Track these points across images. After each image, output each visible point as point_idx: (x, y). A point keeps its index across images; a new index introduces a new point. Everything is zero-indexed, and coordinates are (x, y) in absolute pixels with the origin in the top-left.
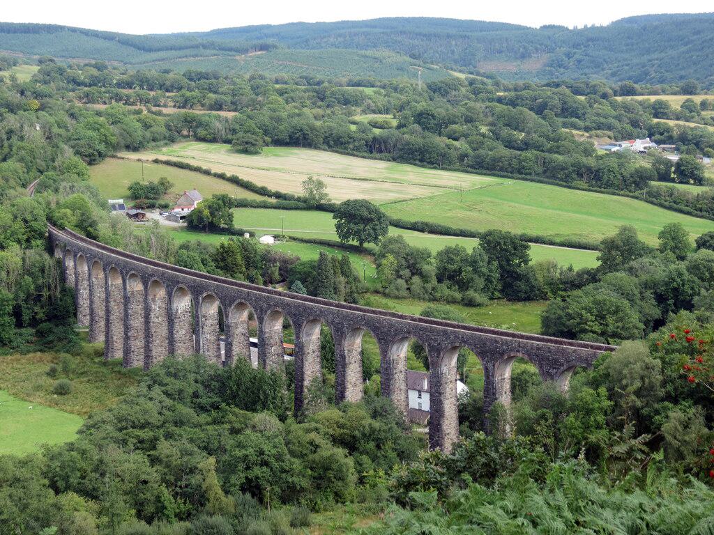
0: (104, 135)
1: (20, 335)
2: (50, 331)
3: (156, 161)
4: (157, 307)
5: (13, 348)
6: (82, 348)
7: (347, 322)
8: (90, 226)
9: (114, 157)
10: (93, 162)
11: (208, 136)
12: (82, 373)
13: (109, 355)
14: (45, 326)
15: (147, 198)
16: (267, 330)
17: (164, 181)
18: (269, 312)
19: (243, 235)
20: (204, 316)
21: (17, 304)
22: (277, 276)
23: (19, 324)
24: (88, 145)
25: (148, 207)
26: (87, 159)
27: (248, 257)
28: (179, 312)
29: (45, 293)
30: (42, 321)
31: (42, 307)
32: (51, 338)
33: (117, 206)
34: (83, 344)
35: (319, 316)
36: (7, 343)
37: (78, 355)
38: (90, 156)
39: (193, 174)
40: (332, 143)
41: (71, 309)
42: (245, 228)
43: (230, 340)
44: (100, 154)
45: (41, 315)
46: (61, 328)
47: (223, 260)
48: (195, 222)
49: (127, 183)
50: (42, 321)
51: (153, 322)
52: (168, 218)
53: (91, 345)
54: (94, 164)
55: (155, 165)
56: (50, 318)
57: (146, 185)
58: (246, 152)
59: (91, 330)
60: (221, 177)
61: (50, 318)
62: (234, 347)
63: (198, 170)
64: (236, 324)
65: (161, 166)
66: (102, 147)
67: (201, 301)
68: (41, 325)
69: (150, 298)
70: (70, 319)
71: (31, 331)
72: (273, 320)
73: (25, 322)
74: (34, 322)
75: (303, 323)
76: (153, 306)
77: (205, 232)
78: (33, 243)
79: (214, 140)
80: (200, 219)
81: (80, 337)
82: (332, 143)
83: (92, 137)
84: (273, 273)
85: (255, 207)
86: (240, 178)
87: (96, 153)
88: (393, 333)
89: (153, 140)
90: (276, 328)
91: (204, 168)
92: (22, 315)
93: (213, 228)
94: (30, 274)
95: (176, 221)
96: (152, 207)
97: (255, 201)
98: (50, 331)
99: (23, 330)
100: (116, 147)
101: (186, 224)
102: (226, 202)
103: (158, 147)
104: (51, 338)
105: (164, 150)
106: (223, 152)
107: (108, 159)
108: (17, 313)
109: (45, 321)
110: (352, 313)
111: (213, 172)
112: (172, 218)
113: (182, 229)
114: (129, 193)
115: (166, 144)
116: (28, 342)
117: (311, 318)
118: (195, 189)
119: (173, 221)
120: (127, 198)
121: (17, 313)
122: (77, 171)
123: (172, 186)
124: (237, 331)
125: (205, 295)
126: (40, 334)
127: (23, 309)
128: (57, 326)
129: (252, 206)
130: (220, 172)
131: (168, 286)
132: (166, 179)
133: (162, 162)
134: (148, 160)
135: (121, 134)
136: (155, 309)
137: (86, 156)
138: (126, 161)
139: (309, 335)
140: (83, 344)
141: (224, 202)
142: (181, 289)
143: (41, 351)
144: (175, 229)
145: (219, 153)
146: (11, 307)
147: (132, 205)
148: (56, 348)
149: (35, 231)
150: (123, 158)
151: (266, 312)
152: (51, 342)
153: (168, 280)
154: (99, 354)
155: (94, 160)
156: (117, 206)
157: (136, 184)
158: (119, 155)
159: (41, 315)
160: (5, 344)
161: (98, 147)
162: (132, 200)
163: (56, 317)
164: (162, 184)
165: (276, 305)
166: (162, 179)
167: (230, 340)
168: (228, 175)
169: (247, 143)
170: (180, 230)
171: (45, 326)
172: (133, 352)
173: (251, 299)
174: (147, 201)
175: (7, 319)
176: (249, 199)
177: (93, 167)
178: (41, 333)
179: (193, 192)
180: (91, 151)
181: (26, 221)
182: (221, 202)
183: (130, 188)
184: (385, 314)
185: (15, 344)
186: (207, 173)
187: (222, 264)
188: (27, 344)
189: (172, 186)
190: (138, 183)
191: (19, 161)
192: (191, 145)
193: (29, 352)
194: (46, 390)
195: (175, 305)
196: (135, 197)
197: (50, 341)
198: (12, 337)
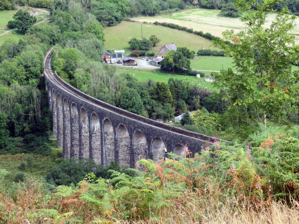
0: (121, 6)
1: (13, 141)
2: (32, 139)
3: (156, 24)
4: (85, 126)
5: (7, 150)
6: (51, 151)
7: (173, 140)
8: (72, 70)
9: (128, 20)
10: (111, 24)
11: (208, 5)
12: (42, 168)
13: (65, 156)
14: (29, 136)
15: (141, 49)
16: (135, 144)
17: (153, 38)
18: (135, 132)
19: (196, 75)
20: (106, 133)
21: (11, 121)
22: (198, 104)
23: (13, 135)
24: (109, 13)
25: (140, 56)
26: (107, 22)
27: (178, 92)
28: (96, 129)
29: (31, 114)
30: (28, 133)
31: (29, 124)
32: (32, 144)
33: (117, 55)
34: (53, 148)
35: (159, 135)
36: (3, 146)
37: (47, 155)
38: (109, 20)
39: (180, 32)
40: (294, 9)
41: (49, 125)
42: (198, 71)
43: (117, 150)
44: (116, 18)
45: (27, 129)
46: (40, 138)
47: (157, 94)
48: (165, 66)
49: (130, 38)
50: (28, 133)
51: (84, 136)
52: (151, 63)
53: (57, 149)
54: (112, 26)
55: (155, 26)
56: (33, 131)
57: (140, 41)
58: (230, 15)
59: (58, 140)
60: (200, 34)
61: (33, 131)
62: (120, 154)
63: (184, 29)
64: (121, 139)
65: (159, 27)
66: (118, 14)
67: (103, 123)
68: (27, 135)
69: (81, 120)
70: (48, 132)
71: (21, 139)
72: (139, 137)
73: (16, 133)
74: (23, 134)
75: (151, 140)
76: (84, 125)
77: (172, 73)
78: (30, 81)
79: (212, 8)
80: (169, 65)
81: (53, 143)
82: (294, 9)
83: (111, 8)
84: (195, 103)
85: (216, 56)
86: (212, 35)
87: (113, 18)
88: (196, 149)
89: (170, 8)
90: (141, 142)
91: (188, 28)
92: (15, 129)
93: (178, 71)
94: (20, 102)
95: (155, 65)
96: (142, 55)
97: (216, 51)
98: (32, 139)
99: (16, 139)
100: (132, 14)
101: (159, 68)
102: (186, 54)
103: (170, 12)
104: (32, 144)
105: (174, 14)
106: (215, 16)
107: (123, 22)
108: (11, 127)
109: (30, 133)
110: (175, 134)
111: (194, 31)
112: (153, 63)
113: (157, 70)
114: (129, 46)
115: (177, 10)
116: (17, 147)
117: (155, 137)
118: (173, 43)
119: (153, 65)
120: (127, 49)
121: (11, 127)
122: (95, 31)
123: (158, 41)
124: (122, 144)
125: (105, 119)
126: (26, 141)
127: (15, 125)
128: (38, 136)
129: (213, 55)
130: (198, 30)
131: (88, 113)
132: (155, 36)
133: (160, 24)
134: (150, 23)
135: (136, 5)
136: (85, 127)
137: (106, 20)
138: (135, 23)
139: (156, 148)
140: (53, 148)
141: (183, 52)
142: (94, 114)
143: (25, 152)
144: (153, 71)
145: (212, 16)
146: (5, 124)
147: (129, 54)
148: (35, 151)
149: (32, 73)
150: (134, 21)
151: (133, 131)
152: (33, 147)
153: (88, 108)
154: (60, 155)
155: (112, 23)
156: (117, 55)
157: (133, 40)
158: (132, 19)
159: (27, 129)
160: (2, 148)
161: (116, 14)
162: (131, 51)
163: (38, 130)
164: (152, 40)
165: (138, 128)
166: (152, 36)
167: (117, 150)
168: (204, 33)
169: (231, 10)
170: (155, 72)
171: (29, 136)
172: (76, 155)
173: (126, 123)
174: (140, 51)
175: (3, 131)
176: (212, 50)
177: (111, 28)
178: (27, 140)
179: (172, 45)
180: (110, 17)
181: (26, 67)
182: (181, 53)
183: (130, 43)
184: (191, 135)
185: (8, 148)
186: (190, 31)
187: (156, 96)
188: (16, 147)
189: (158, 41)
190: (135, 39)
191: (57, 24)
192: (195, 11)
193: (17, 153)
194: (11, 179)
195: (92, 125)
196: (133, 48)
197: (32, 146)
198: (7, 143)
